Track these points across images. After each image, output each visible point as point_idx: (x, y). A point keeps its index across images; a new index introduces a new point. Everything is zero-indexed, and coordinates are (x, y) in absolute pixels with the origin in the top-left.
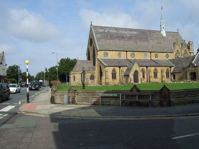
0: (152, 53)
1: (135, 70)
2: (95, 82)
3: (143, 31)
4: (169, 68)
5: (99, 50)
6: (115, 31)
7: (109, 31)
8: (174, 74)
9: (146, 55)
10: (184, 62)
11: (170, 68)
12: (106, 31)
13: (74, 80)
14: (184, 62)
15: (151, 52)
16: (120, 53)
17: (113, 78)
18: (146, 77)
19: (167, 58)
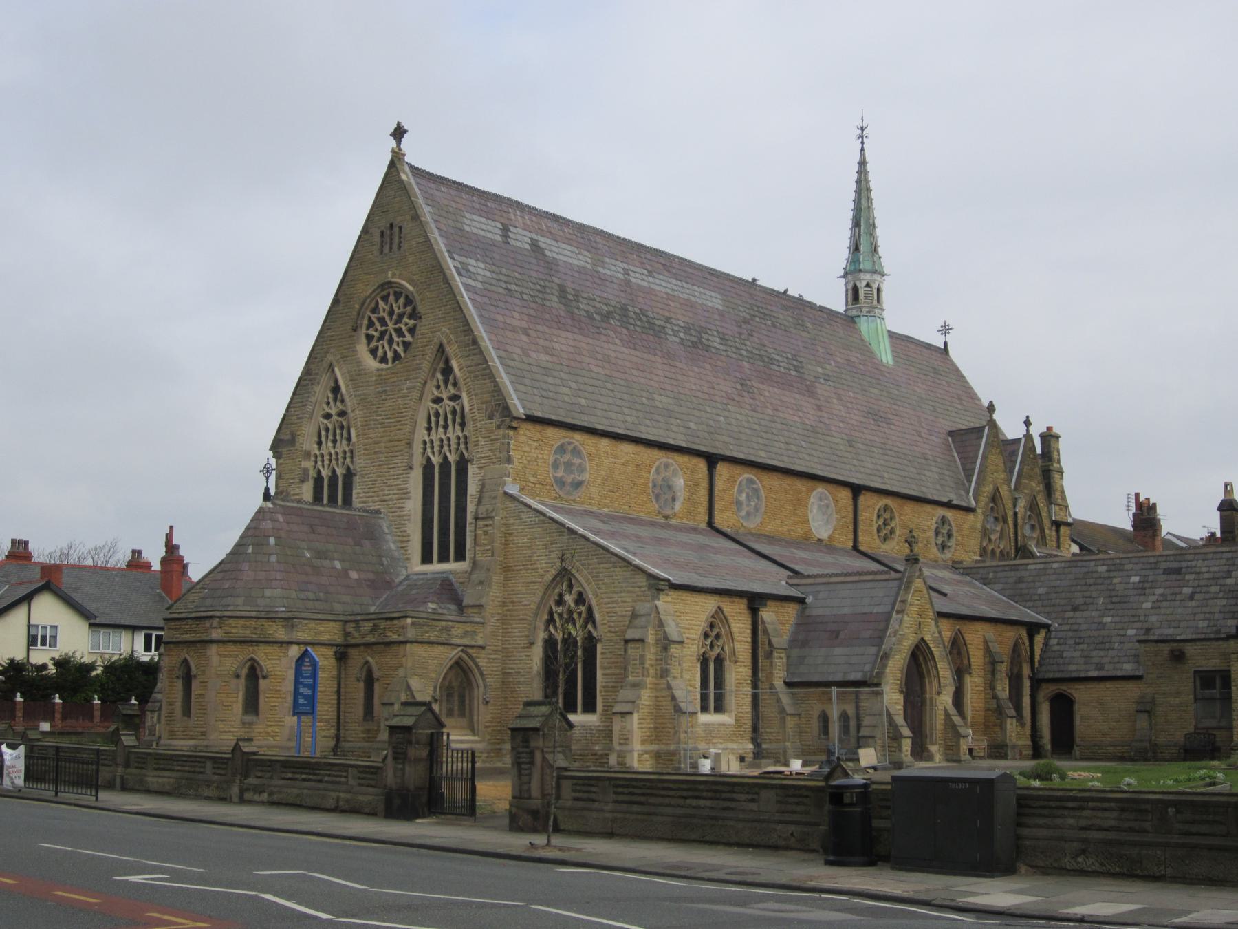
0: (722, 469)
1: (908, 644)
2: (938, 757)
3: (564, 254)
4: (1024, 633)
5: (520, 411)
6: (582, 260)
7: (543, 242)
8: (1064, 687)
9: (800, 504)
10: (1142, 589)
11: (1031, 638)
12: (521, 238)
13: (187, 711)
14: (1142, 589)
15: (712, 460)
16: (667, 466)
17: (184, 715)
18: (325, 708)
19: (943, 547)
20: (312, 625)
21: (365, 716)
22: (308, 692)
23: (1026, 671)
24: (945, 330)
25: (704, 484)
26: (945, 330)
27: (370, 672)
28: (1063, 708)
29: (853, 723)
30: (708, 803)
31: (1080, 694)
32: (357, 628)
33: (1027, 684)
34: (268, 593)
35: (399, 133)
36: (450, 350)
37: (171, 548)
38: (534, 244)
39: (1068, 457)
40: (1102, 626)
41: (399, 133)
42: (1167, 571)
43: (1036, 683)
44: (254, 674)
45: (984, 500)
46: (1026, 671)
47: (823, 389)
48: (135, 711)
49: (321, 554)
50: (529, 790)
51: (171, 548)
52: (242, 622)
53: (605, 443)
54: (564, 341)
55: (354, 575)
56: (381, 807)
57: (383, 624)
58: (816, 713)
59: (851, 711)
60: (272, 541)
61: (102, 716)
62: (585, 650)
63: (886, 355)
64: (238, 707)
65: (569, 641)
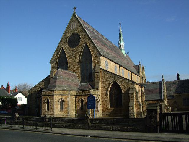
22: (91, 104)
35: (75, 8)
37: (8, 85)
41: (75, 8)
42: (174, 84)
51: (8, 85)
55: (74, 83)
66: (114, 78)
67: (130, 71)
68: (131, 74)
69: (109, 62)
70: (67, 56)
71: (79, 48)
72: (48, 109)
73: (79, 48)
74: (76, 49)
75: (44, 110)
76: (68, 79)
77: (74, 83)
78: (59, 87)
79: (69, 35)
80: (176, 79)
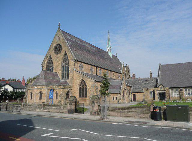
6: (80, 43)
7: (76, 40)
8: (134, 93)
14: (142, 82)
20: (49, 87)
21: (40, 98)
22: (51, 95)
23: (130, 92)
24: (117, 54)
25: (96, 70)
26: (117, 54)
27: (57, 93)
28: (134, 96)
29: (117, 98)
30: (127, 110)
31: (136, 94)
32: (55, 87)
33: (130, 93)
34: (43, 82)
35: (60, 25)
36: (67, 52)
37: (23, 79)
38: (75, 40)
39: (130, 68)
40: (138, 87)
41: (60, 25)
42: (145, 80)
43: (131, 93)
44: (41, 94)
45: (123, 73)
46: (130, 92)
47: (106, 59)
48: (158, 109)
49: (50, 78)
50: (94, 109)
51: (23, 79)
52: (40, 86)
53: (85, 64)
54: (80, 52)
55: (54, 80)
56: (68, 112)
57: (59, 86)
58: (113, 97)
59: (117, 97)
60: (43, 76)
61: (184, 121)
62: (85, 89)
63: (111, 56)
64: (39, 98)
65: (83, 89)
66: (82, 77)
67: (110, 70)
68: (111, 72)
69: (83, 64)
70: (54, 60)
71: (62, 55)
72: (31, 99)
73: (62, 55)
74: (58, 55)
75: (29, 99)
76: (50, 78)
77: (54, 80)
78: (40, 83)
79: (54, 45)
80: (149, 77)
